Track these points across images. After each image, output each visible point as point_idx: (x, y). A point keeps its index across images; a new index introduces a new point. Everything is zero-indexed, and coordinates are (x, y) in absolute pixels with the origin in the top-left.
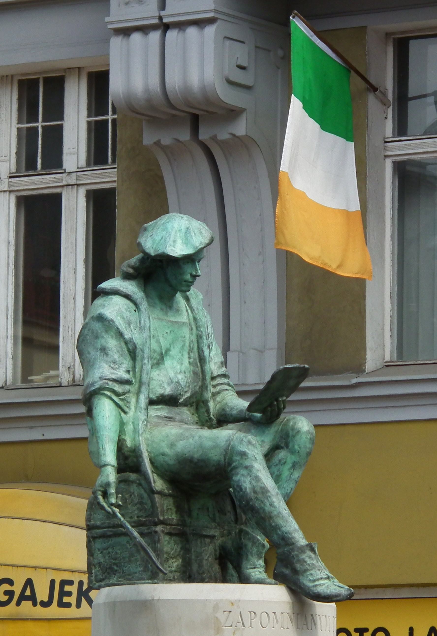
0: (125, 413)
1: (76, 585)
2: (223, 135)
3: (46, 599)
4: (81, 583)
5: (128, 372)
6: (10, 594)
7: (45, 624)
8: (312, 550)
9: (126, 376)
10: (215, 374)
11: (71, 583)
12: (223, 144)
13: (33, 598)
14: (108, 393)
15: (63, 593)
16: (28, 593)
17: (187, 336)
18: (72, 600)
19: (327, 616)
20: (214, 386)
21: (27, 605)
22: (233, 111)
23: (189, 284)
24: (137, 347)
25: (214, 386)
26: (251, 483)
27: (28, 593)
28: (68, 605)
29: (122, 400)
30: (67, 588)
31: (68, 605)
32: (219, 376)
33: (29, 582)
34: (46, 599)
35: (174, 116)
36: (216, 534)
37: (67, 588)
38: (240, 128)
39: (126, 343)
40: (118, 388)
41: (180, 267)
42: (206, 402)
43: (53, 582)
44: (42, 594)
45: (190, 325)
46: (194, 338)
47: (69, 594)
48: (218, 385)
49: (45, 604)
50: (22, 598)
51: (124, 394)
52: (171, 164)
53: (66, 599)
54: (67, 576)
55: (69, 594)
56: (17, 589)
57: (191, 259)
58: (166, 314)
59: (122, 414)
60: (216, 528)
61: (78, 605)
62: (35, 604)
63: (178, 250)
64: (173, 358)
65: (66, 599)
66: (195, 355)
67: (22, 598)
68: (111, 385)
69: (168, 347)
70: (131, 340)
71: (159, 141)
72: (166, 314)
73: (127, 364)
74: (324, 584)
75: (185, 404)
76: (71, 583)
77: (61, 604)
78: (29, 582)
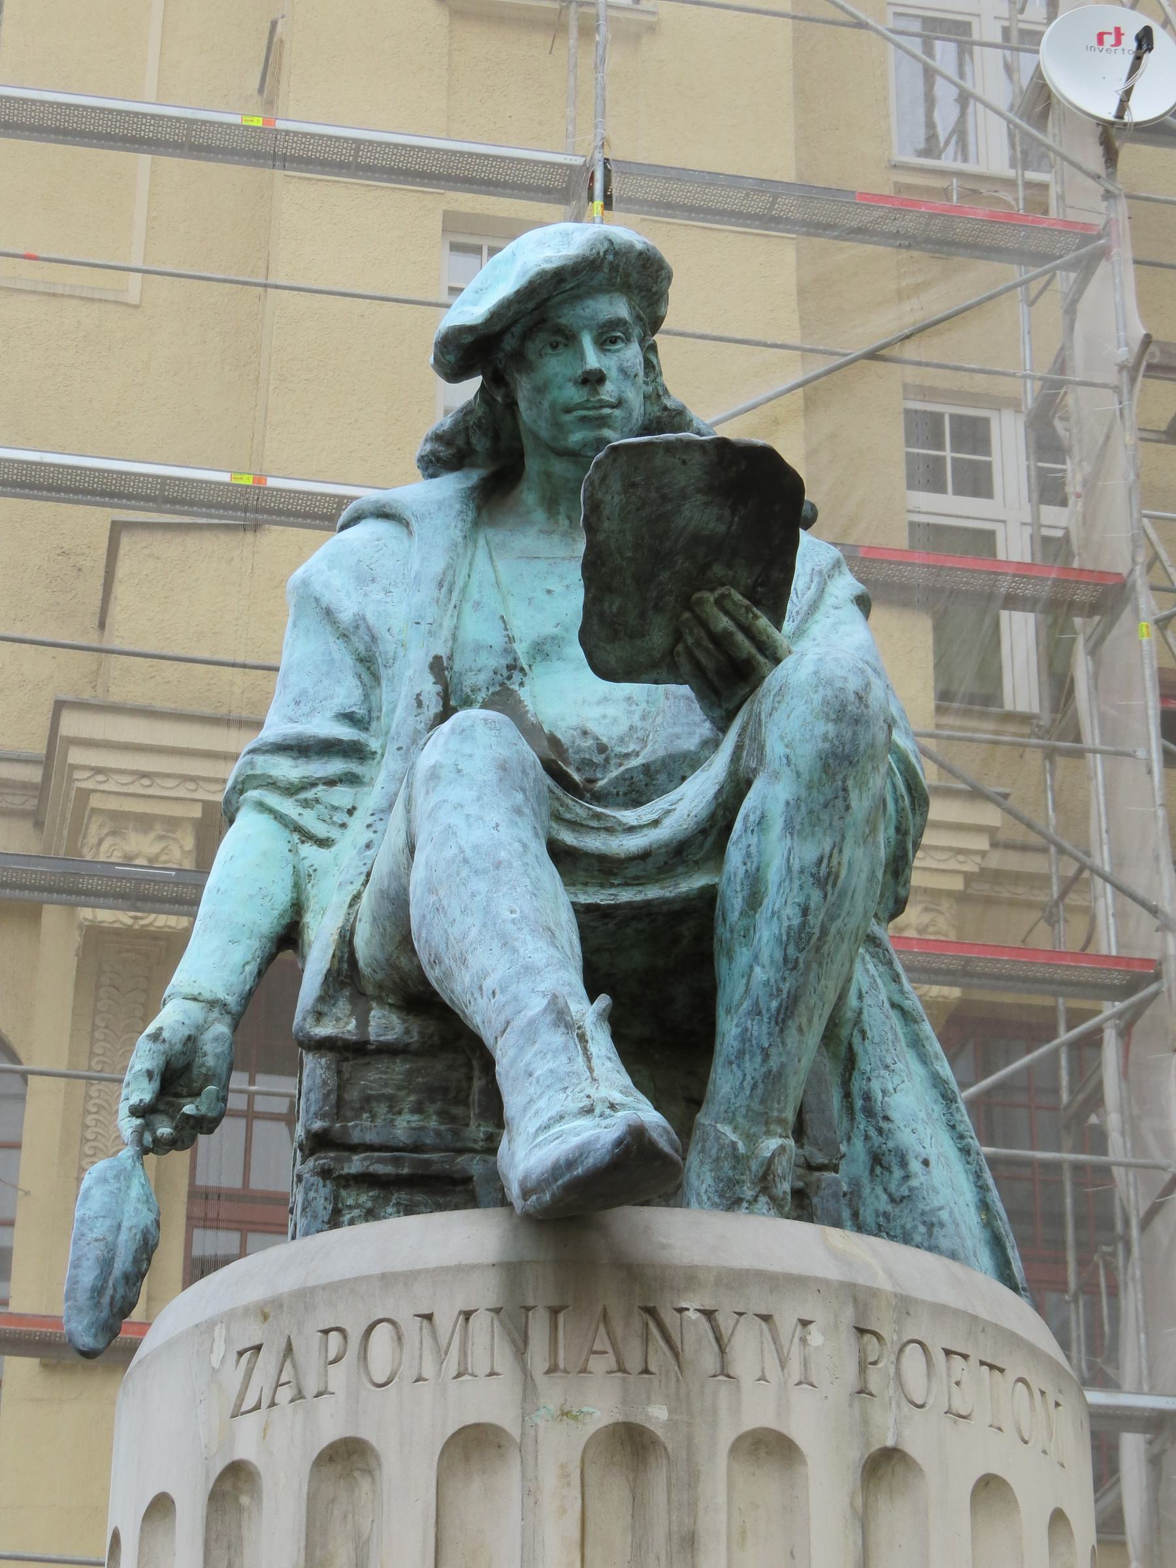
5: (349, 718)
9: (345, 732)
19: (786, 1322)
29: (306, 804)
39: (344, 636)
59: (308, 850)
70: (360, 621)
73: (346, 692)
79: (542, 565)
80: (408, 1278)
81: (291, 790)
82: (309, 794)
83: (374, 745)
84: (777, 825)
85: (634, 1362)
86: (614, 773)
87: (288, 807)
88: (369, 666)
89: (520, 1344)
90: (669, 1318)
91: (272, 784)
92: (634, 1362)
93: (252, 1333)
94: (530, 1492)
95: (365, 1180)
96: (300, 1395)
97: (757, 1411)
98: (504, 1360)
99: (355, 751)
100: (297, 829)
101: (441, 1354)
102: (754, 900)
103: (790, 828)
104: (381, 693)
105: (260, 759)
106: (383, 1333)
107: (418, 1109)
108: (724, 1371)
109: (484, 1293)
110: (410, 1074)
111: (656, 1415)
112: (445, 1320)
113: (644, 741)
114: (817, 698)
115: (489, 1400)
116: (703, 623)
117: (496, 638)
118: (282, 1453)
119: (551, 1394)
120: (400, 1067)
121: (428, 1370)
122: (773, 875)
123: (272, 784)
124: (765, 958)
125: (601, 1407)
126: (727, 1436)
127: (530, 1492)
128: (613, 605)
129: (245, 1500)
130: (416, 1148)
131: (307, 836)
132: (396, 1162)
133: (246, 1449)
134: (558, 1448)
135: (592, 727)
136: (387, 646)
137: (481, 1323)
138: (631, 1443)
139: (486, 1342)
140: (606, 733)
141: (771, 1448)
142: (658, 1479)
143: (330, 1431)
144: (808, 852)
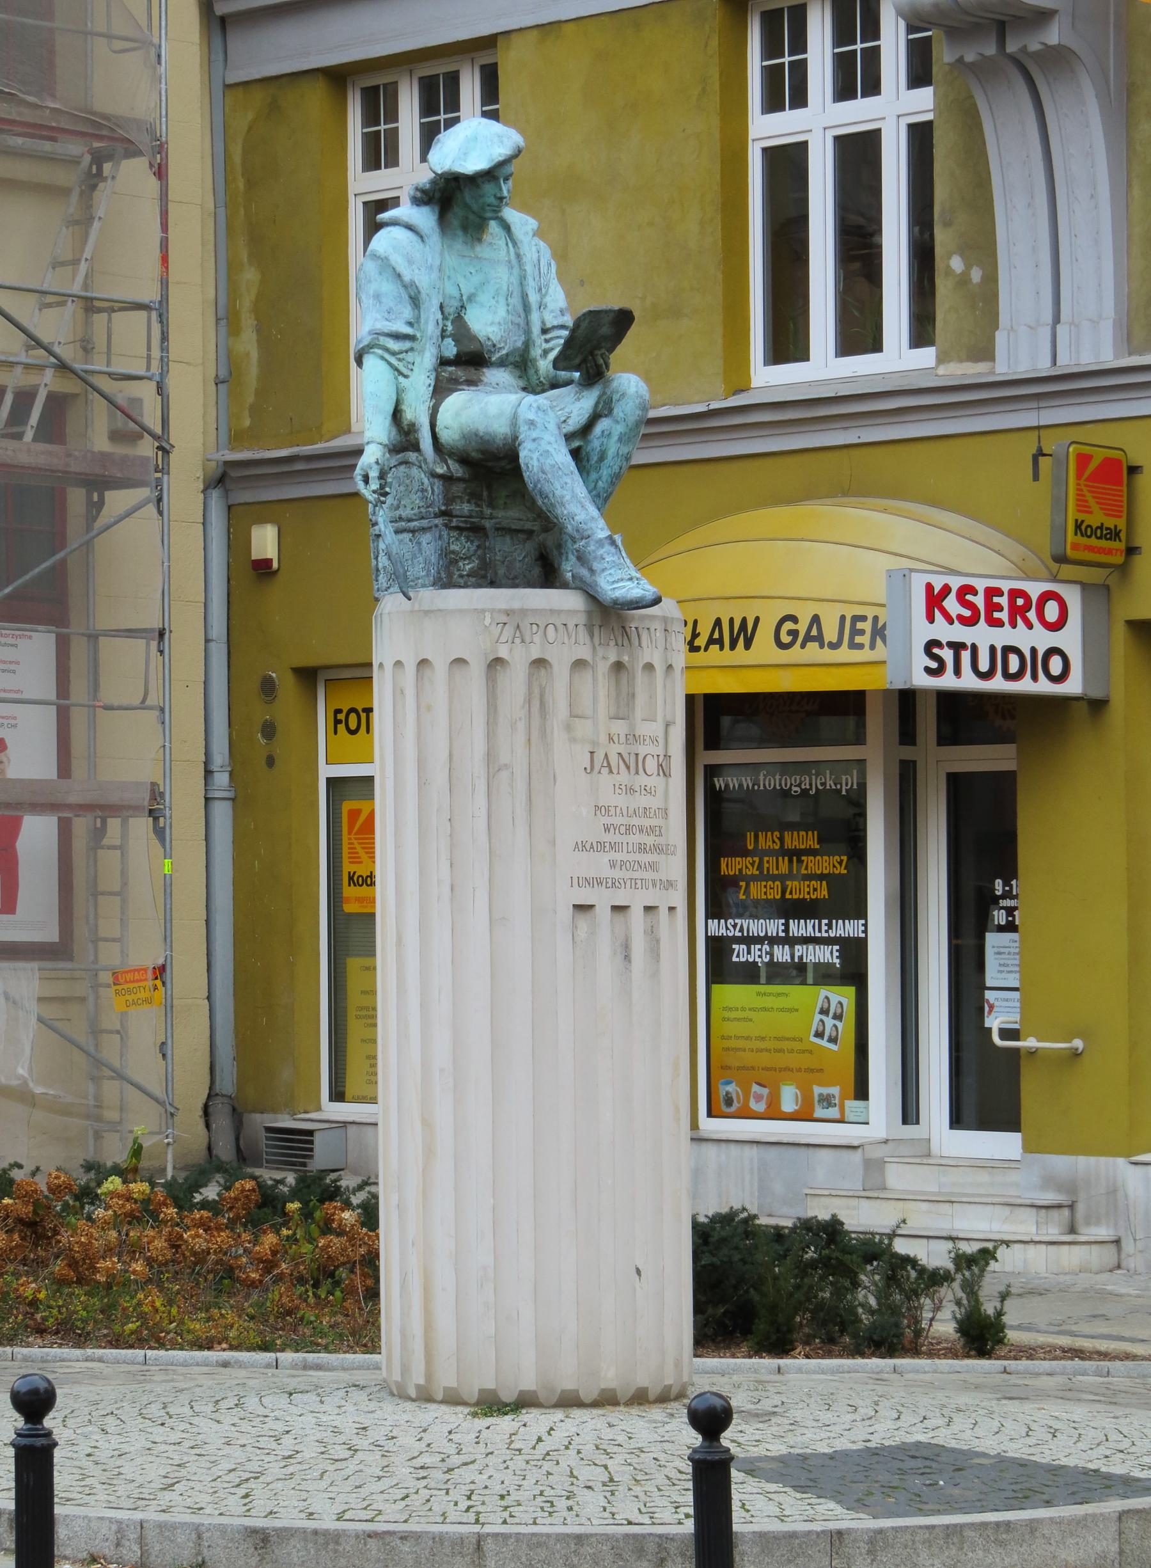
0: (406, 377)
1: (870, 620)
2: (1034, 46)
3: (835, 640)
4: (876, 618)
5: (410, 324)
6: (794, 633)
7: (824, 669)
8: (613, 543)
9: (408, 330)
10: (549, 325)
11: (863, 618)
12: (1036, 56)
13: (820, 639)
14: (380, 352)
15: (855, 632)
16: (814, 632)
17: (505, 277)
18: (865, 639)
19: (652, 630)
20: (547, 341)
21: (813, 646)
22: (1043, 13)
23: (497, 210)
24: (422, 291)
25: (547, 341)
26: (538, 460)
27: (814, 632)
28: (861, 646)
29: (399, 360)
30: (860, 625)
31: (861, 646)
32: (554, 328)
33: (816, 619)
34: (835, 640)
35: (977, 24)
36: (535, 528)
37: (860, 625)
38: (1053, 35)
39: (405, 287)
40: (393, 345)
41: (478, 186)
42: (534, 361)
43: (843, 618)
44: (830, 635)
45: (509, 262)
46: (515, 280)
47: (862, 632)
48: (552, 339)
49: (834, 646)
50: (808, 638)
51: (401, 352)
52: (982, 87)
53: (858, 639)
54: (859, 611)
55: (862, 632)
56: (802, 627)
57: (491, 175)
58: (473, 247)
59: (401, 379)
60: (534, 520)
61: (873, 646)
62: (822, 646)
63: (473, 164)
64: (482, 305)
65: (858, 639)
66: (516, 301)
67: (808, 638)
68: (383, 341)
69: (473, 291)
70: (413, 283)
71: (962, 57)
72: (473, 247)
73: (407, 312)
74: (624, 587)
75: (502, 363)
76: (863, 618)
77: (853, 646)
78: (816, 619)
79: (467, 260)
80: (559, 612)
81: (393, 354)
82: (401, 356)
83: (418, 335)
84: (615, 438)
85: (620, 643)
86: (498, 355)
87: (393, 360)
88: (415, 301)
89: (592, 635)
90: (628, 630)
91: (387, 350)
92: (620, 643)
93: (504, 619)
94: (595, 679)
95: (457, 528)
96: (523, 641)
97: (647, 659)
98: (587, 639)
99: (411, 338)
100: (397, 370)
101: (569, 637)
102: (602, 458)
103: (620, 440)
104: (507, 389)
105: (381, 338)
106: (551, 627)
107: (469, 502)
108: (640, 645)
109: (581, 619)
110: (465, 489)
111: (625, 659)
112: (571, 626)
113: (506, 343)
114: (637, 402)
115: (584, 652)
116: (595, 361)
117: (456, 294)
118: (518, 658)
119: (601, 652)
120: (462, 486)
121: (566, 641)
122: (611, 453)
123: (387, 350)
124: (604, 479)
125: (613, 658)
126: (641, 665)
127: (595, 679)
128: (569, 352)
129: (498, 668)
130: (470, 517)
131: (401, 373)
132: (466, 522)
133: (503, 652)
134: (603, 667)
135: (491, 336)
136: (423, 296)
137: (581, 628)
138: (618, 666)
139: (583, 635)
140: (495, 338)
141: (649, 667)
142: (624, 677)
143: (535, 655)
144: (625, 450)
